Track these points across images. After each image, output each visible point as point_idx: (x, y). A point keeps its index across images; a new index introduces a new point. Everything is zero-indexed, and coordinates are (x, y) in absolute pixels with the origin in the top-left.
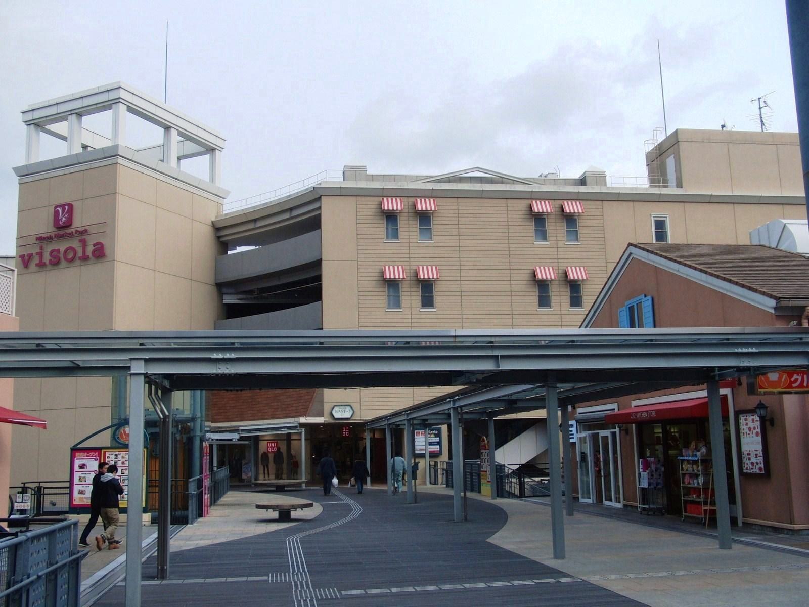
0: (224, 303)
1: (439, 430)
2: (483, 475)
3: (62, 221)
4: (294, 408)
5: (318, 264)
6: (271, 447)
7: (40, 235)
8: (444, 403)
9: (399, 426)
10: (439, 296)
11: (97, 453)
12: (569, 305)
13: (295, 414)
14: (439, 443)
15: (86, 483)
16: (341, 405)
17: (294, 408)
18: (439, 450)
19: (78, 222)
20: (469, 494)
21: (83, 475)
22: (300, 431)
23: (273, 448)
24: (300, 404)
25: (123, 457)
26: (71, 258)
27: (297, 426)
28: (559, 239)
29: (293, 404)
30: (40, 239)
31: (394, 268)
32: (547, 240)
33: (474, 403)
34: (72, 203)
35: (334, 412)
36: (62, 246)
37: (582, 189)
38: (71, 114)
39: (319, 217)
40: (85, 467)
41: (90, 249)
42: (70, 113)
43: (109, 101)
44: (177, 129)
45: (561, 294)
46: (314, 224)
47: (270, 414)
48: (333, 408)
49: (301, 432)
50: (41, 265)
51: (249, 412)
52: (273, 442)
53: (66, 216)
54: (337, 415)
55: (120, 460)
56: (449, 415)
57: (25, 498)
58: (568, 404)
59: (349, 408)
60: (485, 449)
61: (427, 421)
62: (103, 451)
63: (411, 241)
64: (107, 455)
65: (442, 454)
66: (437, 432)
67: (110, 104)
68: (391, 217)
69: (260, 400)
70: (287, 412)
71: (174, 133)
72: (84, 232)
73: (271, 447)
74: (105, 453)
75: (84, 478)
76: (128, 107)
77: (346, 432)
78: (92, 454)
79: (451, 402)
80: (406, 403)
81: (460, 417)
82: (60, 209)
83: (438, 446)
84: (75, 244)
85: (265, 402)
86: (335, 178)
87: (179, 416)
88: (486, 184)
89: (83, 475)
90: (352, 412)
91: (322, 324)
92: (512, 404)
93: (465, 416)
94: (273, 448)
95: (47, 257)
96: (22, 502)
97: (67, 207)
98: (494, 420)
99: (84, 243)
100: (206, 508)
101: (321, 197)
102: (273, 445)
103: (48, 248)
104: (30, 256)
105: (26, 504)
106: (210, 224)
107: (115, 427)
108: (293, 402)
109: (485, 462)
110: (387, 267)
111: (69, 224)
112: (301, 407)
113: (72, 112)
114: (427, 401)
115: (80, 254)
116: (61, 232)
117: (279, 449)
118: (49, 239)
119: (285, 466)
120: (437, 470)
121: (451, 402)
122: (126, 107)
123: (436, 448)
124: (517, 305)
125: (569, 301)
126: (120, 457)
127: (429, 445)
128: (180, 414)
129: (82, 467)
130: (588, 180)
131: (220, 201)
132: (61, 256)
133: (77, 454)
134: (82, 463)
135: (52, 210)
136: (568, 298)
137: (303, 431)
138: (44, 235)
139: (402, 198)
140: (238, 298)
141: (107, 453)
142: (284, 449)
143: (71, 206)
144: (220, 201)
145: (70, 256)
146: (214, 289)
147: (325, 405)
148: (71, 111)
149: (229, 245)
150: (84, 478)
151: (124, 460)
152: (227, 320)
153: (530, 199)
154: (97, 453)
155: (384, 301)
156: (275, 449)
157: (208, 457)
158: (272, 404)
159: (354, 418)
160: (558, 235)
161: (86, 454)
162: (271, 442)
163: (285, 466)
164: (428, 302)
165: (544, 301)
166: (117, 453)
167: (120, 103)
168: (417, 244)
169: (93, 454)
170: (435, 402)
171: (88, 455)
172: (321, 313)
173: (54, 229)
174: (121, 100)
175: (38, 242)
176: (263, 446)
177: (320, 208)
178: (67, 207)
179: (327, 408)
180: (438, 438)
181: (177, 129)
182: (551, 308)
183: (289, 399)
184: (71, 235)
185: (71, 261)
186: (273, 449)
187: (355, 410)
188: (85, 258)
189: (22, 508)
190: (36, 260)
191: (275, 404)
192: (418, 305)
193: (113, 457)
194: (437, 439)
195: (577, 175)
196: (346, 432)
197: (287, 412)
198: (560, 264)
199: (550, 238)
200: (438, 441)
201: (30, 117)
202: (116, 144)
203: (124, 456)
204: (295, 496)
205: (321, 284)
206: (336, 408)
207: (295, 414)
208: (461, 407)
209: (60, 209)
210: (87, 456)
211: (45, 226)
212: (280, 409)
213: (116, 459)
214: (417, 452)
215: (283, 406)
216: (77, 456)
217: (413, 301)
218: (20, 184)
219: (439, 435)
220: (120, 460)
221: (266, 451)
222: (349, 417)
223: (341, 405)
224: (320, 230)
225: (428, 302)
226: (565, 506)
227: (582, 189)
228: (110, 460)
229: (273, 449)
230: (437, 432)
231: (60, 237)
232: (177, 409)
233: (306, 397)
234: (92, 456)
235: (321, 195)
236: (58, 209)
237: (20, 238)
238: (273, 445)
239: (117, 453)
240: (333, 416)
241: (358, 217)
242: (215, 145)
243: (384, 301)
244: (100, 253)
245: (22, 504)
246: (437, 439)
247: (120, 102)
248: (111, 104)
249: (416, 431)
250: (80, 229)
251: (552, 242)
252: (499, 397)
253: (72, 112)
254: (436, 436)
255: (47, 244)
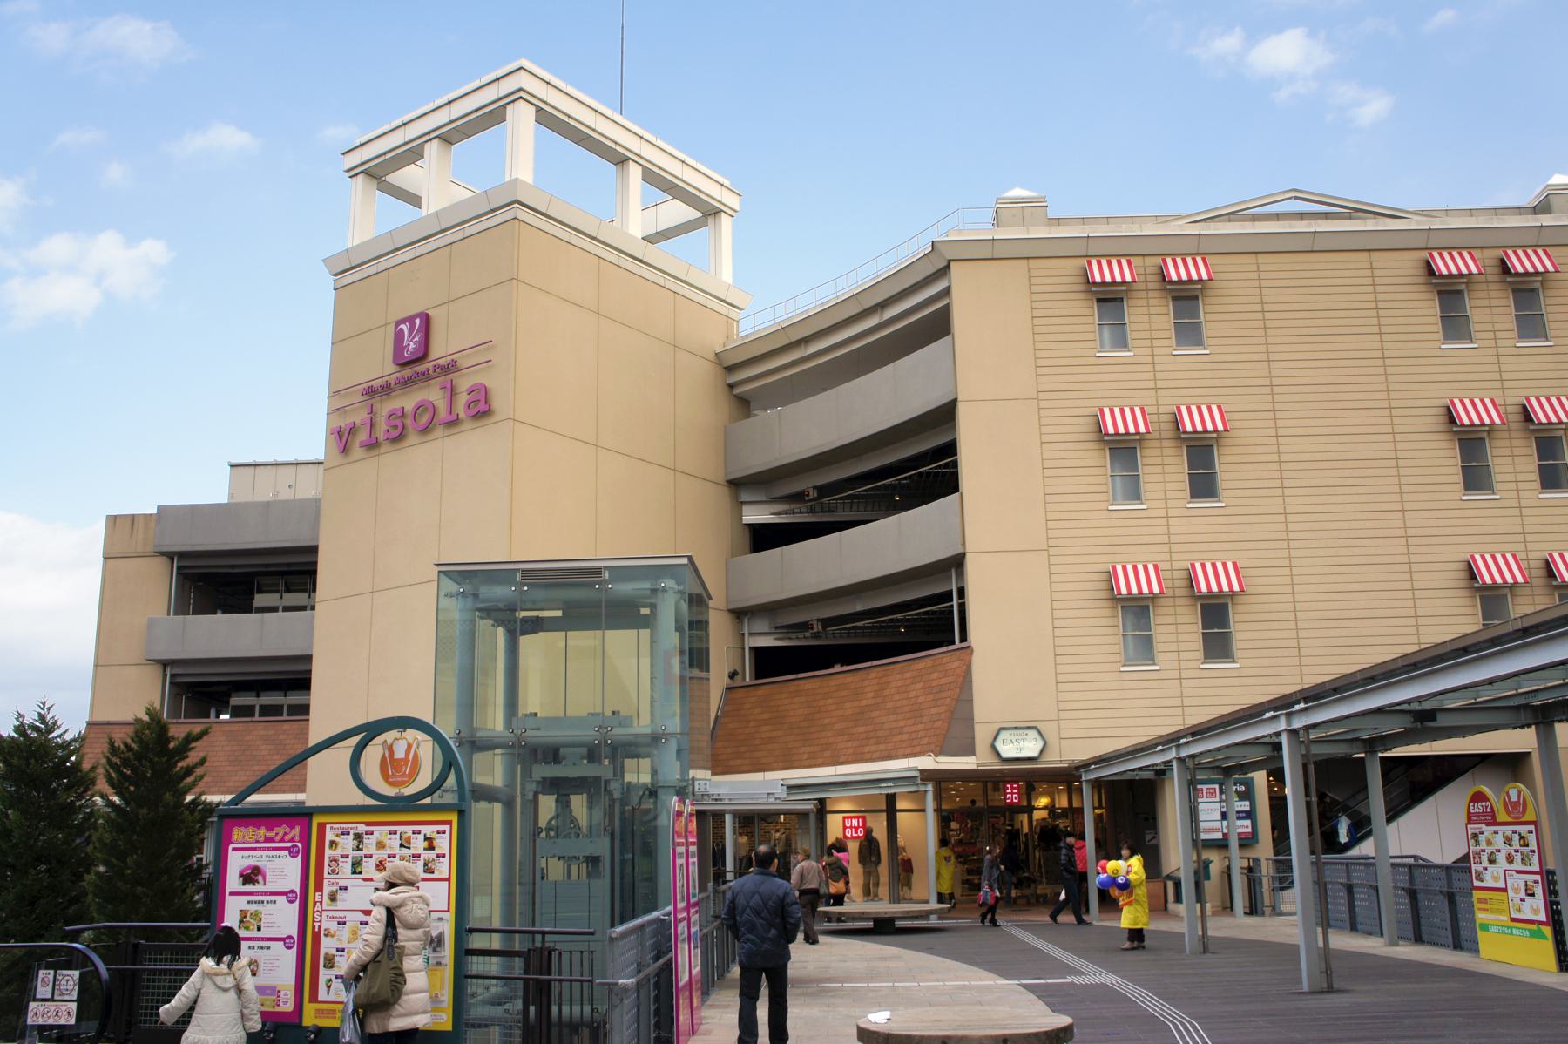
0: (744, 522)
1: (1249, 784)
2: (1481, 901)
3: (408, 350)
4: (905, 737)
5: (945, 415)
6: (851, 827)
7: (370, 384)
8: (1259, 722)
9: (1434, 719)
10: (1226, 469)
11: (297, 830)
12: (1537, 485)
13: (908, 750)
14: (1249, 815)
15: (260, 934)
16: (1016, 728)
17: (905, 737)
18: (1249, 830)
19: (440, 350)
20: (1343, 941)
21: (253, 907)
22: (922, 788)
23: (856, 829)
24: (921, 727)
25: (381, 845)
26: (428, 423)
27: (916, 777)
28: (1499, 335)
29: (902, 727)
30: (371, 392)
31: (1122, 411)
32: (1471, 339)
33: (1210, 751)
34: (427, 312)
35: (999, 745)
36: (407, 402)
37: (1546, 220)
38: (431, 140)
39: (946, 311)
40: (260, 878)
41: (462, 399)
42: (427, 138)
43: (500, 99)
44: (641, 165)
45: (1517, 460)
46: (937, 326)
47: (850, 751)
48: (997, 735)
49: (926, 791)
50: (372, 445)
51: (803, 750)
52: (855, 817)
53: (417, 338)
54: (1008, 749)
55: (371, 856)
56: (1277, 747)
57: (63, 986)
58: (1379, 749)
59: (1033, 733)
60: (1494, 823)
61: (1434, 719)
62: (316, 821)
63: (1156, 351)
64: (330, 835)
65: (1257, 842)
66: (1243, 788)
67: (502, 106)
68: (1109, 299)
69: (826, 721)
70: (890, 746)
71: (635, 172)
72: (450, 368)
73: (851, 827)
74: (322, 827)
75: (256, 915)
76: (539, 110)
77: (1012, 793)
78: (280, 830)
79: (1174, 749)
80: (1228, 700)
81: (1304, 752)
82: (405, 327)
83: (1248, 822)
84: (434, 394)
85: (837, 727)
86: (975, 226)
87: (617, 731)
88: (1320, 222)
89: (253, 907)
90: (1040, 744)
91: (964, 544)
92: (1424, 720)
93: (1316, 750)
94: (856, 829)
95: (382, 427)
96: (52, 1000)
97: (418, 321)
98: (1381, 758)
99: (452, 392)
100: (683, 1003)
101: (948, 267)
102: (855, 823)
103: (385, 407)
104: (353, 429)
105: (64, 1007)
106: (712, 357)
107: (355, 740)
108: (901, 724)
109: (1492, 861)
110: (1107, 412)
111: (423, 356)
112: (921, 734)
113: (432, 135)
114: (1224, 715)
115: (442, 413)
116: (407, 373)
117: (868, 832)
118: (386, 390)
119: (883, 869)
120: (1260, 879)
121: (1174, 749)
122: (533, 109)
123: (1244, 826)
124: (1413, 488)
125: (1536, 476)
126: (370, 844)
127: (1239, 818)
128: (621, 725)
129: (251, 876)
130: (1554, 201)
131: (733, 313)
132: (408, 422)
133: (237, 832)
134: (253, 862)
135: (391, 330)
136: (1534, 468)
137: (930, 787)
138: (376, 384)
139: (1132, 259)
140: (775, 511)
141: (328, 827)
142: (880, 833)
143: (426, 319)
144: (733, 313)
145: (424, 419)
146: (725, 492)
147: (977, 728)
148: (429, 133)
149: (752, 404)
150: (256, 915)
151: (383, 854)
152: (752, 555)
153: (1426, 249)
154: (297, 830)
155: (1103, 488)
156: (861, 832)
157: (693, 849)
158: (855, 730)
159: (1045, 758)
160: (1498, 327)
161: (263, 832)
162: (851, 818)
163: (883, 869)
164: (1203, 486)
165: (1476, 478)
166: (362, 828)
167: (521, 100)
168: (1171, 359)
169: (285, 834)
170: (1415, 666)
171: (271, 834)
172: (958, 519)
173: (393, 368)
174: (522, 94)
175: (365, 397)
176: (835, 827)
177: (946, 292)
178: (418, 321)
179: (982, 735)
180: (1247, 803)
181: (641, 165)
182: (1494, 493)
183: (892, 717)
184: (425, 377)
185: (426, 430)
186: (856, 832)
187: (1047, 740)
188: (453, 422)
189: (51, 1021)
190: (363, 436)
191: (861, 729)
192: (1180, 495)
193: (347, 843)
194: (1244, 806)
195: (1529, 198)
196: (1012, 793)
197: (890, 746)
198: (1507, 392)
199: (1478, 335)
200: (1248, 809)
201: (355, 159)
202: (513, 177)
203: (385, 839)
204: (930, 950)
205: (955, 464)
206: (1004, 735)
207: (908, 750)
208: (1193, 756)
209: (405, 327)
210: (268, 840)
211: (381, 366)
212: (872, 741)
213: (358, 849)
214: (1204, 836)
215: (881, 733)
216: (235, 838)
217: (1169, 486)
218: (335, 290)
219: (1248, 795)
220: (371, 856)
221: (840, 835)
222: (1034, 753)
223: (1016, 728)
224: (948, 338)
225: (1203, 486)
226: (695, 840)
227: (1546, 220)
228: (338, 852)
229: (856, 832)
230: (1243, 788)
231: (405, 383)
232: (614, 713)
233: (934, 711)
234: (282, 840)
235: (949, 261)
236: (403, 326)
237: (335, 393)
238: (855, 823)
239: (362, 828)
240: (998, 753)
241: (1035, 305)
242: (720, 202)
243: (1103, 488)
244: (481, 408)
245: (51, 1006)
246: (1244, 806)
247: (521, 98)
248: (504, 106)
249: (1217, 787)
250: (442, 362)
251: (1486, 343)
252: (1257, 738)
253: (432, 135)
254: (1243, 796)
255: (381, 400)
